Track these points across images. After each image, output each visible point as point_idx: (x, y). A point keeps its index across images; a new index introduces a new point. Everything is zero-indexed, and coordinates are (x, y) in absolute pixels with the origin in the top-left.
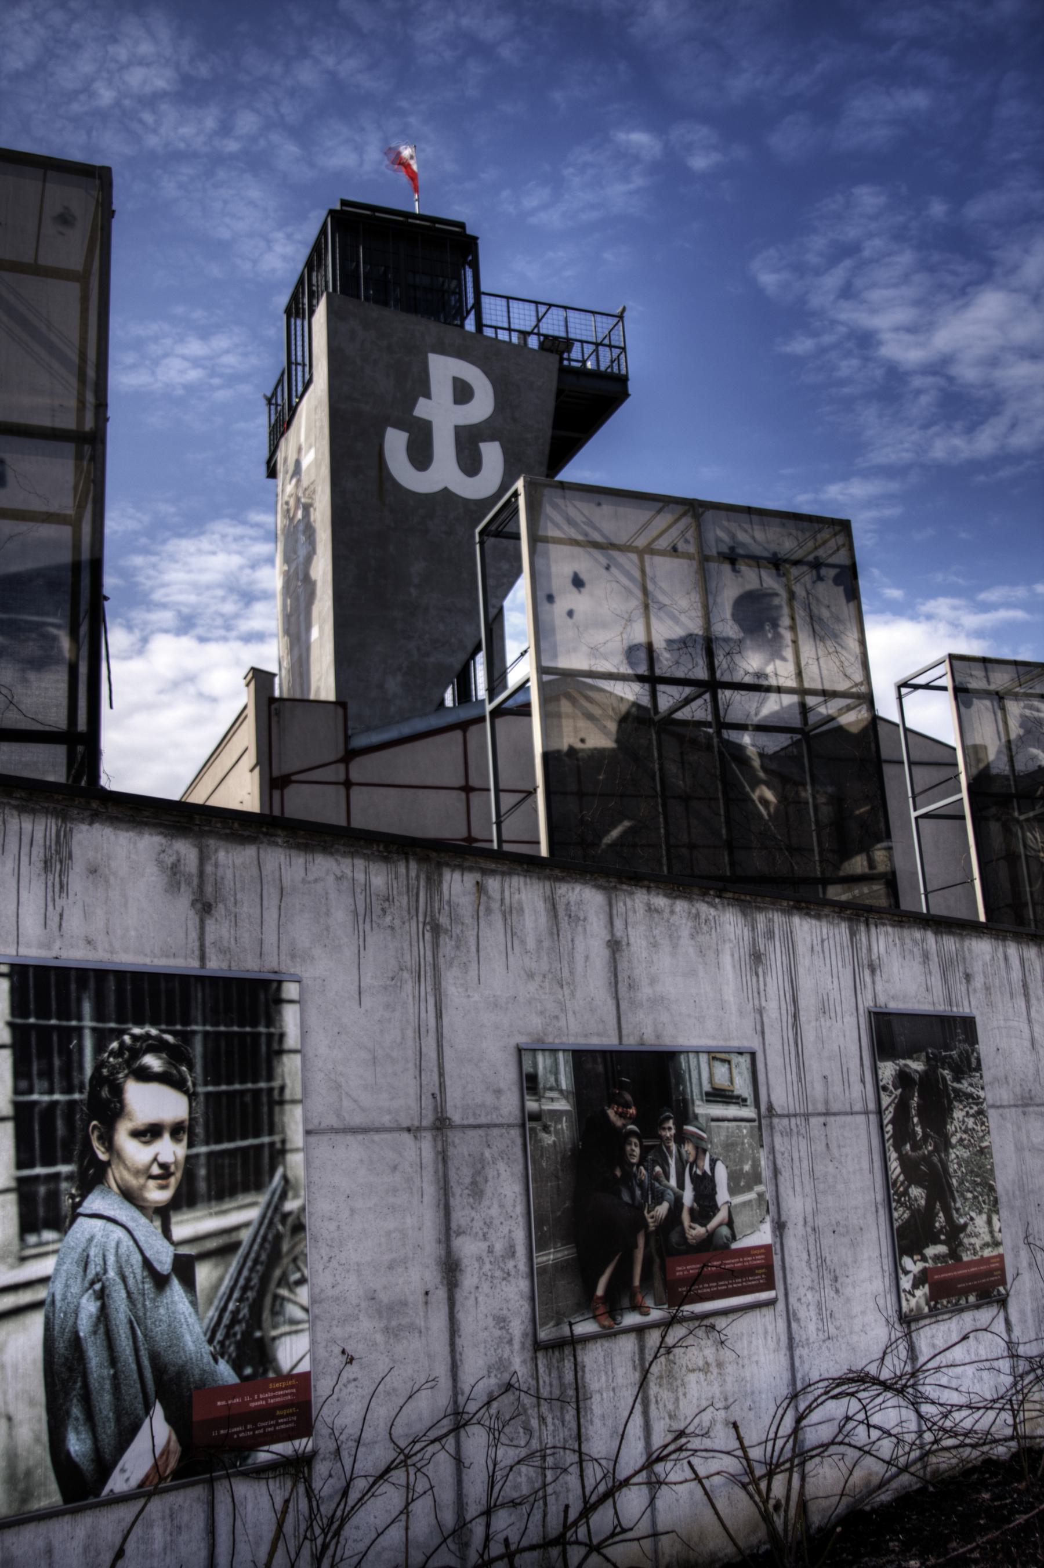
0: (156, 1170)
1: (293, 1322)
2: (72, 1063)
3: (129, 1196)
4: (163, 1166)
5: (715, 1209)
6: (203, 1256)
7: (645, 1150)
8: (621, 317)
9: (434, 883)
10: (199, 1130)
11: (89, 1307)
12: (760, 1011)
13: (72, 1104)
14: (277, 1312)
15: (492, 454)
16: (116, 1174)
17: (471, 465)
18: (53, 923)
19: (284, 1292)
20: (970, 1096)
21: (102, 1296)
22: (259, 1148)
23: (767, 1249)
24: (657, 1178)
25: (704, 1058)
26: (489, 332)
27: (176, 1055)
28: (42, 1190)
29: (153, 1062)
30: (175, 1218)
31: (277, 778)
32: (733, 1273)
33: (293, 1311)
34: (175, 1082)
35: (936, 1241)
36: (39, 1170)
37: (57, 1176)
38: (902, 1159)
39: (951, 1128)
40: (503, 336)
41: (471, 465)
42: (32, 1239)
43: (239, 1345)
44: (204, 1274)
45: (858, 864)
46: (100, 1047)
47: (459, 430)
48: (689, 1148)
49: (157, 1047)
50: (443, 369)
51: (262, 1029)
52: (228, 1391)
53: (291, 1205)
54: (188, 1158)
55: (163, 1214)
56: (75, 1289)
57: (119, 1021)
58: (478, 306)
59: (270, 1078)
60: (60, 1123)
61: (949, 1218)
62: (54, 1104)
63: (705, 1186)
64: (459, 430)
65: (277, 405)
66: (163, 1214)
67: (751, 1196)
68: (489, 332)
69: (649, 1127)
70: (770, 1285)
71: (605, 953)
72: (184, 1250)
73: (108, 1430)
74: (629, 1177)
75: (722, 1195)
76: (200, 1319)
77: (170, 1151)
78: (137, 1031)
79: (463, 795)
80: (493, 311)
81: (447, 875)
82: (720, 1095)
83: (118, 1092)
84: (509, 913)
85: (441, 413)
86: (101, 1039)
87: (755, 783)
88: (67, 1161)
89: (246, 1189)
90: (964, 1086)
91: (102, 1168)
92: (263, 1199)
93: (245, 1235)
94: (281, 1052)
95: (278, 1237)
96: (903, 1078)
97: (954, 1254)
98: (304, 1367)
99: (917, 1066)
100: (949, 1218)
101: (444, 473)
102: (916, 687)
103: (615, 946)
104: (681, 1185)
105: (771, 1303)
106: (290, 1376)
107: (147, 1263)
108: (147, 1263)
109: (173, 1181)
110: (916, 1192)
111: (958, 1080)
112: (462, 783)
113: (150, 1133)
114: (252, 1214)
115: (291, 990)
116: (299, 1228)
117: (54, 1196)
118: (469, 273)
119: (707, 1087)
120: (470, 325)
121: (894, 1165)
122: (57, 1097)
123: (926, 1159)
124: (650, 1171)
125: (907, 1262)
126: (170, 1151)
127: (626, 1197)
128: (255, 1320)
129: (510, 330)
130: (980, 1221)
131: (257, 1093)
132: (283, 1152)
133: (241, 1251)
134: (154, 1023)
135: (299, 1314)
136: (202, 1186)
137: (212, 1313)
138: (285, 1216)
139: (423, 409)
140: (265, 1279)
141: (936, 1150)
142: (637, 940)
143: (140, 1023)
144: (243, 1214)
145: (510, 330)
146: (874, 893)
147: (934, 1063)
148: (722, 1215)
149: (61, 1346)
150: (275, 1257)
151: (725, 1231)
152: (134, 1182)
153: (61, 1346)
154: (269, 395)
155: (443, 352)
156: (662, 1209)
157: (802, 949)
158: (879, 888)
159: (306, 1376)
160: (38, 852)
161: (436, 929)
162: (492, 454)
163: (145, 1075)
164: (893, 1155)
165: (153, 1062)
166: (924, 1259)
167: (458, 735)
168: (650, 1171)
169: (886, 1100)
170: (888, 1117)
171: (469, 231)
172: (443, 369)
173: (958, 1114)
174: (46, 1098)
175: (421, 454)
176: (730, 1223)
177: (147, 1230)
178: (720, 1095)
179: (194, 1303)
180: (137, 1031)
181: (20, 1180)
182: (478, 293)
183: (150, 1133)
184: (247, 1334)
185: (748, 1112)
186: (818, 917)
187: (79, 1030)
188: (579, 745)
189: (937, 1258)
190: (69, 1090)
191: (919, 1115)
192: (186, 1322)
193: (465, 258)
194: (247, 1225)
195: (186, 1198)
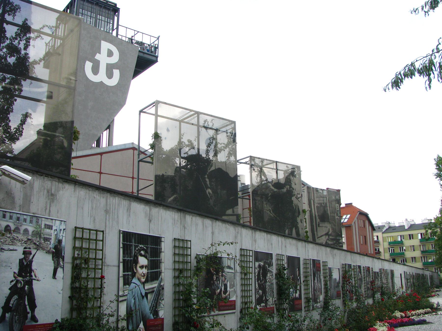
0: (143, 275)
1: (162, 308)
2: (131, 252)
3: (139, 279)
4: (144, 274)
5: (227, 291)
6: (149, 293)
7: (217, 278)
8: (158, 39)
9: (185, 217)
10: (149, 267)
11: (133, 301)
12: (236, 249)
13: (131, 260)
14: (159, 305)
15: (116, 73)
16: (137, 275)
17: (110, 75)
18: (128, 222)
19: (160, 301)
20: (271, 271)
21: (135, 299)
22: (158, 271)
23: (235, 301)
24: (218, 284)
25: (226, 259)
26: (119, 37)
27: (146, 251)
28: (126, 277)
29: (142, 252)
30: (145, 285)
31: (158, 194)
32: (228, 306)
33: (162, 305)
34: (146, 257)
35: (263, 303)
36: (126, 273)
37: (128, 275)
38: (258, 284)
39: (267, 278)
40: (124, 39)
41: (110, 75)
42: (125, 287)
43: (154, 311)
44: (149, 296)
45: (229, 212)
46: (135, 249)
47: (108, 65)
48: (223, 278)
49: (143, 249)
50: (105, 46)
51: (158, 247)
52: (152, 320)
53: (162, 284)
54: (147, 273)
55: (144, 283)
56: (131, 297)
57: (138, 244)
58: (117, 28)
59: (159, 257)
60: (129, 264)
61: (266, 298)
62: (128, 260)
63: (226, 286)
64: (108, 65)
65: (49, 46)
66: (144, 283)
67: (233, 289)
68: (119, 37)
69: (217, 274)
70: (235, 309)
71: (211, 235)
72: (147, 291)
73: (135, 325)
74: (214, 283)
75: (228, 289)
76: (148, 305)
77: (145, 271)
78: (140, 246)
79: (99, 174)
80: (122, 31)
81: (187, 216)
82: (229, 267)
83: (137, 258)
84: (197, 225)
85: (103, 58)
86: (136, 247)
87: (207, 188)
88: (130, 272)
89: (156, 280)
90: (270, 269)
91: (135, 273)
92: (158, 282)
93: (155, 289)
94: (161, 252)
95: (160, 290)
96: (259, 266)
97: (266, 306)
98: (163, 317)
99: (262, 264)
100: (266, 298)
101: (101, 77)
102: (241, 163)
103: (213, 233)
104: (222, 286)
105: (234, 313)
106: (161, 318)
107: (141, 293)
108: (141, 293)
109: (145, 277)
110: (260, 291)
111: (269, 267)
112: (99, 171)
113: (142, 267)
114: (156, 285)
115: (163, 239)
116: (163, 289)
117: (128, 278)
118: (116, 18)
119: (227, 265)
120: (114, 33)
121: (257, 285)
122: (129, 258)
123: (262, 284)
124: (217, 282)
125: (258, 306)
126: (145, 271)
127: (213, 288)
128: (156, 307)
129: (126, 37)
130: (271, 299)
131: (158, 260)
132: (161, 273)
133: (155, 292)
134: (143, 245)
135: (162, 306)
136: (149, 279)
137: (150, 304)
138: (161, 286)
139: (98, 57)
140: (158, 298)
141: (264, 283)
142: (216, 231)
143: (141, 244)
144: (155, 285)
145: (126, 37)
146: (234, 218)
147: (265, 263)
148: (228, 293)
149: (129, 308)
150: (159, 294)
151: (229, 297)
152: (140, 277)
153: (129, 308)
154: (47, 43)
155: (106, 41)
156: (219, 291)
157: (244, 236)
158: (235, 217)
159: (163, 318)
160: (126, 209)
161: (185, 228)
162: (116, 73)
163: (141, 255)
164: (257, 283)
165: (142, 252)
166: (261, 306)
167: (99, 156)
168: (217, 282)
169: (256, 271)
170: (256, 274)
171: (118, 6)
172: (105, 46)
173: (268, 275)
174: (127, 259)
175: (95, 70)
176: (229, 295)
177: (141, 286)
178: (229, 267)
179: (148, 302)
180: (140, 246)
181: (124, 275)
182: (118, 25)
183: (142, 267)
184: (155, 309)
185: (233, 271)
186: (246, 229)
187: (132, 245)
188: (165, 174)
189: (263, 306)
190: (130, 258)
191: (262, 274)
192: (147, 305)
193: (115, 14)
194: (155, 287)
195: (147, 281)
